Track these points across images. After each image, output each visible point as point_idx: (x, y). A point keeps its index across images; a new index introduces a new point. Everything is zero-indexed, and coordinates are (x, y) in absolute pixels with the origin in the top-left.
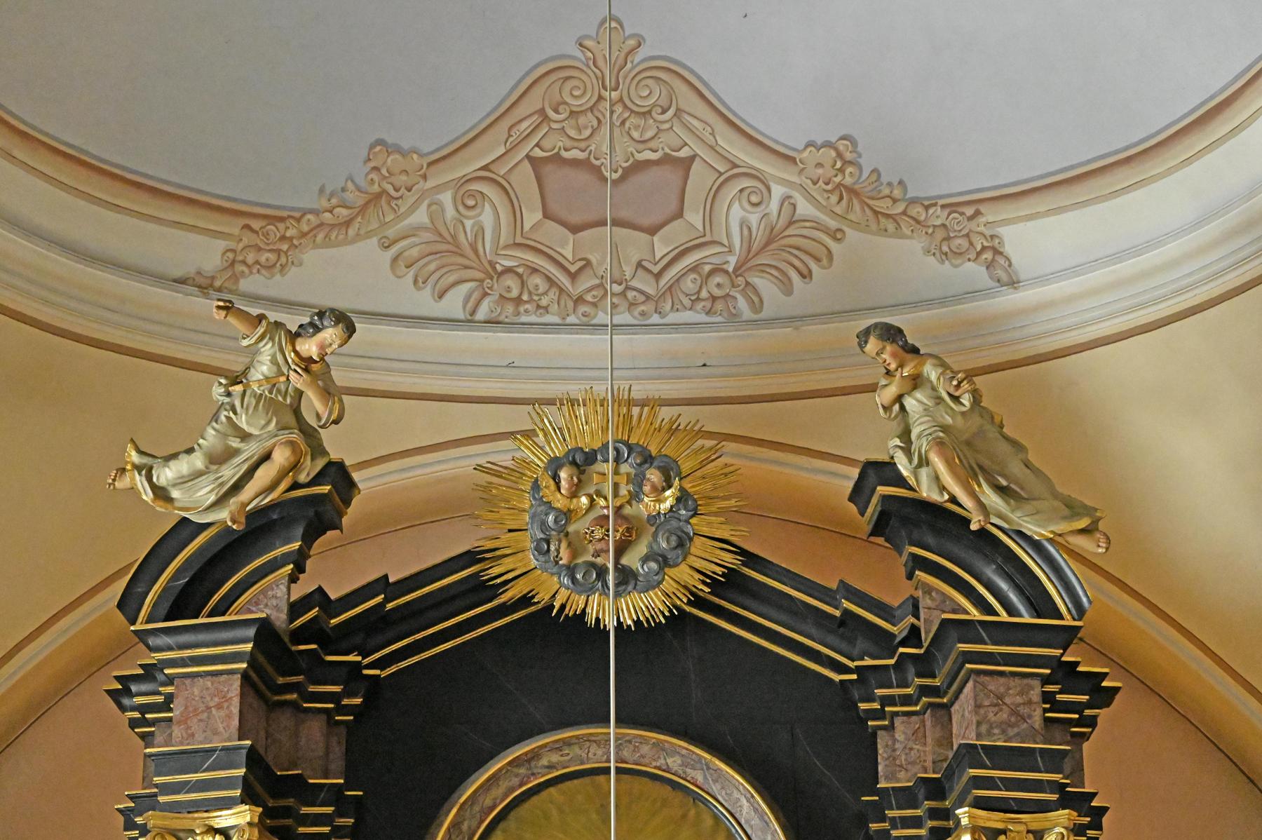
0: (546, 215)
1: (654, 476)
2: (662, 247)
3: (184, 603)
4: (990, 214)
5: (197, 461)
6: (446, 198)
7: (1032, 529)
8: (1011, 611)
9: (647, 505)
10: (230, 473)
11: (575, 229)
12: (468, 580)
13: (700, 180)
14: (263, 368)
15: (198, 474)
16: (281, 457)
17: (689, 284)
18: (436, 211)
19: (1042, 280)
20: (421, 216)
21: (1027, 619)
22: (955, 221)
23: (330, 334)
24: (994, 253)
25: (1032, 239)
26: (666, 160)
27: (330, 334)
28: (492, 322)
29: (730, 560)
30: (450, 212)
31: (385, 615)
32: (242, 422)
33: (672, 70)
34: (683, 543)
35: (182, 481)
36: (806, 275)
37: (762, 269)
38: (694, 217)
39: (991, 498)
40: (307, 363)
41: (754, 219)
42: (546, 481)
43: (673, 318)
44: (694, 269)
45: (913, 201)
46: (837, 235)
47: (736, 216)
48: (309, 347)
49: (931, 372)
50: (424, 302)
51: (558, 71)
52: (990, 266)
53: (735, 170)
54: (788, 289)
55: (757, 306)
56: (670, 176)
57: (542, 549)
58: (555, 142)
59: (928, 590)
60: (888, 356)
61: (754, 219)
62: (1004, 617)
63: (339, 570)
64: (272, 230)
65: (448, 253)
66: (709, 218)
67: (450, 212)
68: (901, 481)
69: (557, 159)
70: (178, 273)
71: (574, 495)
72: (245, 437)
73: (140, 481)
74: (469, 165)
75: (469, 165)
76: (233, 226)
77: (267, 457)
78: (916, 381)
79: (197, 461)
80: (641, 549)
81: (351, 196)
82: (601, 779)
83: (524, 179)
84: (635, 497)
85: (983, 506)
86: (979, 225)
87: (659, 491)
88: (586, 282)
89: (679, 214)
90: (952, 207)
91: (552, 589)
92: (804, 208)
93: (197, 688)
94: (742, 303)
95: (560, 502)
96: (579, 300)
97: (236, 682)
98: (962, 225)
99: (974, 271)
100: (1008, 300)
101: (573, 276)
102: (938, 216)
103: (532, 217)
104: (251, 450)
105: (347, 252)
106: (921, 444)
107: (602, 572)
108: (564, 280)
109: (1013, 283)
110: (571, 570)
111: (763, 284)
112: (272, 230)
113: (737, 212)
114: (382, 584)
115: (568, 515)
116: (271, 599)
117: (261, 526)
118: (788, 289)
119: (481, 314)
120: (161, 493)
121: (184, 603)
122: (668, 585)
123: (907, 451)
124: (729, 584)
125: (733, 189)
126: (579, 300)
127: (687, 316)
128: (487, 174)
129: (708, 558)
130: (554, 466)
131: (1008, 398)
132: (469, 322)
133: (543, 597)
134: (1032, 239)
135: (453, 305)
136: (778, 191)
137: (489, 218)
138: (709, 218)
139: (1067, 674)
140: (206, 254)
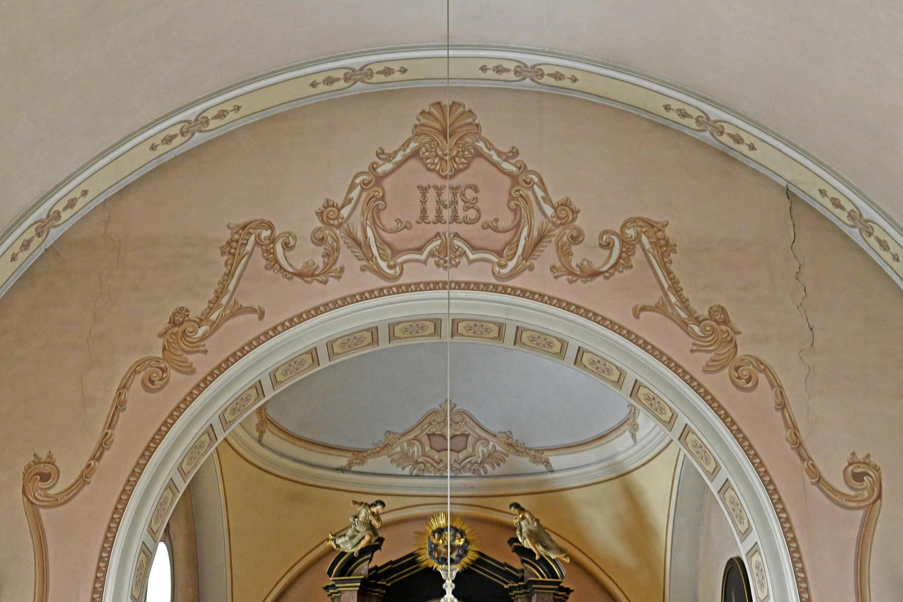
0: (431, 448)
1: (458, 535)
2: (461, 456)
3: (342, 573)
4: (546, 453)
5: (347, 538)
6: (405, 444)
7: (553, 557)
8: (543, 577)
9: (457, 542)
10: (355, 541)
11: (438, 451)
12: (412, 559)
13: (471, 440)
14: (362, 515)
15: (346, 542)
16: (367, 538)
17: (468, 466)
18: (402, 448)
19: (559, 471)
20: (398, 449)
21: (547, 579)
22: (537, 454)
23: (379, 507)
24: (547, 463)
25: (555, 460)
26: (463, 434)
27: (379, 507)
28: (417, 476)
29: (477, 556)
30: (406, 448)
31: (393, 568)
32: (358, 528)
33: (464, 413)
34: (466, 552)
35: (342, 543)
36: (499, 465)
37: (487, 463)
38: (470, 449)
39: (540, 548)
40: (373, 514)
41: (485, 450)
42: (432, 537)
43: (464, 474)
44: (470, 462)
45: (526, 448)
46: (507, 455)
47: (481, 449)
48: (374, 509)
49: (527, 516)
50: (399, 471)
51: (434, 412)
52: (546, 466)
53: (480, 438)
54: (494, 468)
55: (486, 472)
56: (463, 439)
57: (431, 553)
58: (433, 430)
59: (526, 568)
60: (516, 512)
61: (485, 450)
62: (541, 579)
63: (379, 559)
64: (360, 454)
65: (406, 457)
66: (474, 449)
67: (406, 448)
68: (519, 542)
69: (434, 434)
70: (336, 466)
71: (439, 539)
72: (358, 532)
73: (332, 543)
74: (411, 436)
75: (411, 436)
76: (350, 454)
77: (363, 538)
78: (523, 518)
79: (347, 538)
80: (455, 553)
81: (381, 445)
82: (444, 452)
83: (425, 440)
84: (454, 540)
85: (539, 550)
86: (543, 456)
87: (459, 539)
88: (441, 465)
89: (466, 448)
90: (536, 451)
91: (434, 564)
92: (498, 448)
93: (347, 594)
94: (482, 472)
95: (435, 542)
96: (440, 470)
97: (356, 594)
98: (537, 455)
99: (542, 467)
100: (551, 476)
101: (438, 464)
102: (533, 453)
103: (427, 448)
104: (359, 536)
105: (380, 459)
106: (524, 535)
107: (446, 559)
108: (435, 464)
109: (552, 471)
110: (438, 559)
111: (488, 467)
112: (360, 454)
113: (481, 449)
114: (391, 563)
115: (437, 545)
116: (363, 569)
117: (362, 552)
118: (494, 468)
119: (414, 473)
120: (338, 546)
121: (342, 573)
122: (462, 563)
123: (521, 535)
124: (478, 561)
125: (480, 443)
126: (440, 470)
127: (468, 474)
128: (416, 438)
129: (471, 556)
130: (434, 532)
131: (550, 494)
132: (411, 476)
133: (430, 566)
134: (555, 460)
135: (407, 471)
136: (491, 444)
137: (416, 449)
138: (474, 449)
139: (562, 589)
140: (343, 462)
